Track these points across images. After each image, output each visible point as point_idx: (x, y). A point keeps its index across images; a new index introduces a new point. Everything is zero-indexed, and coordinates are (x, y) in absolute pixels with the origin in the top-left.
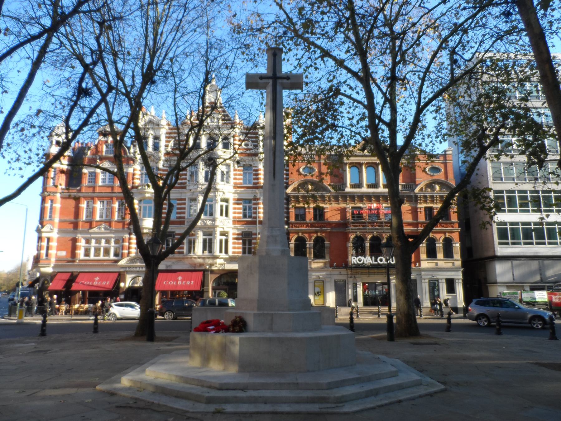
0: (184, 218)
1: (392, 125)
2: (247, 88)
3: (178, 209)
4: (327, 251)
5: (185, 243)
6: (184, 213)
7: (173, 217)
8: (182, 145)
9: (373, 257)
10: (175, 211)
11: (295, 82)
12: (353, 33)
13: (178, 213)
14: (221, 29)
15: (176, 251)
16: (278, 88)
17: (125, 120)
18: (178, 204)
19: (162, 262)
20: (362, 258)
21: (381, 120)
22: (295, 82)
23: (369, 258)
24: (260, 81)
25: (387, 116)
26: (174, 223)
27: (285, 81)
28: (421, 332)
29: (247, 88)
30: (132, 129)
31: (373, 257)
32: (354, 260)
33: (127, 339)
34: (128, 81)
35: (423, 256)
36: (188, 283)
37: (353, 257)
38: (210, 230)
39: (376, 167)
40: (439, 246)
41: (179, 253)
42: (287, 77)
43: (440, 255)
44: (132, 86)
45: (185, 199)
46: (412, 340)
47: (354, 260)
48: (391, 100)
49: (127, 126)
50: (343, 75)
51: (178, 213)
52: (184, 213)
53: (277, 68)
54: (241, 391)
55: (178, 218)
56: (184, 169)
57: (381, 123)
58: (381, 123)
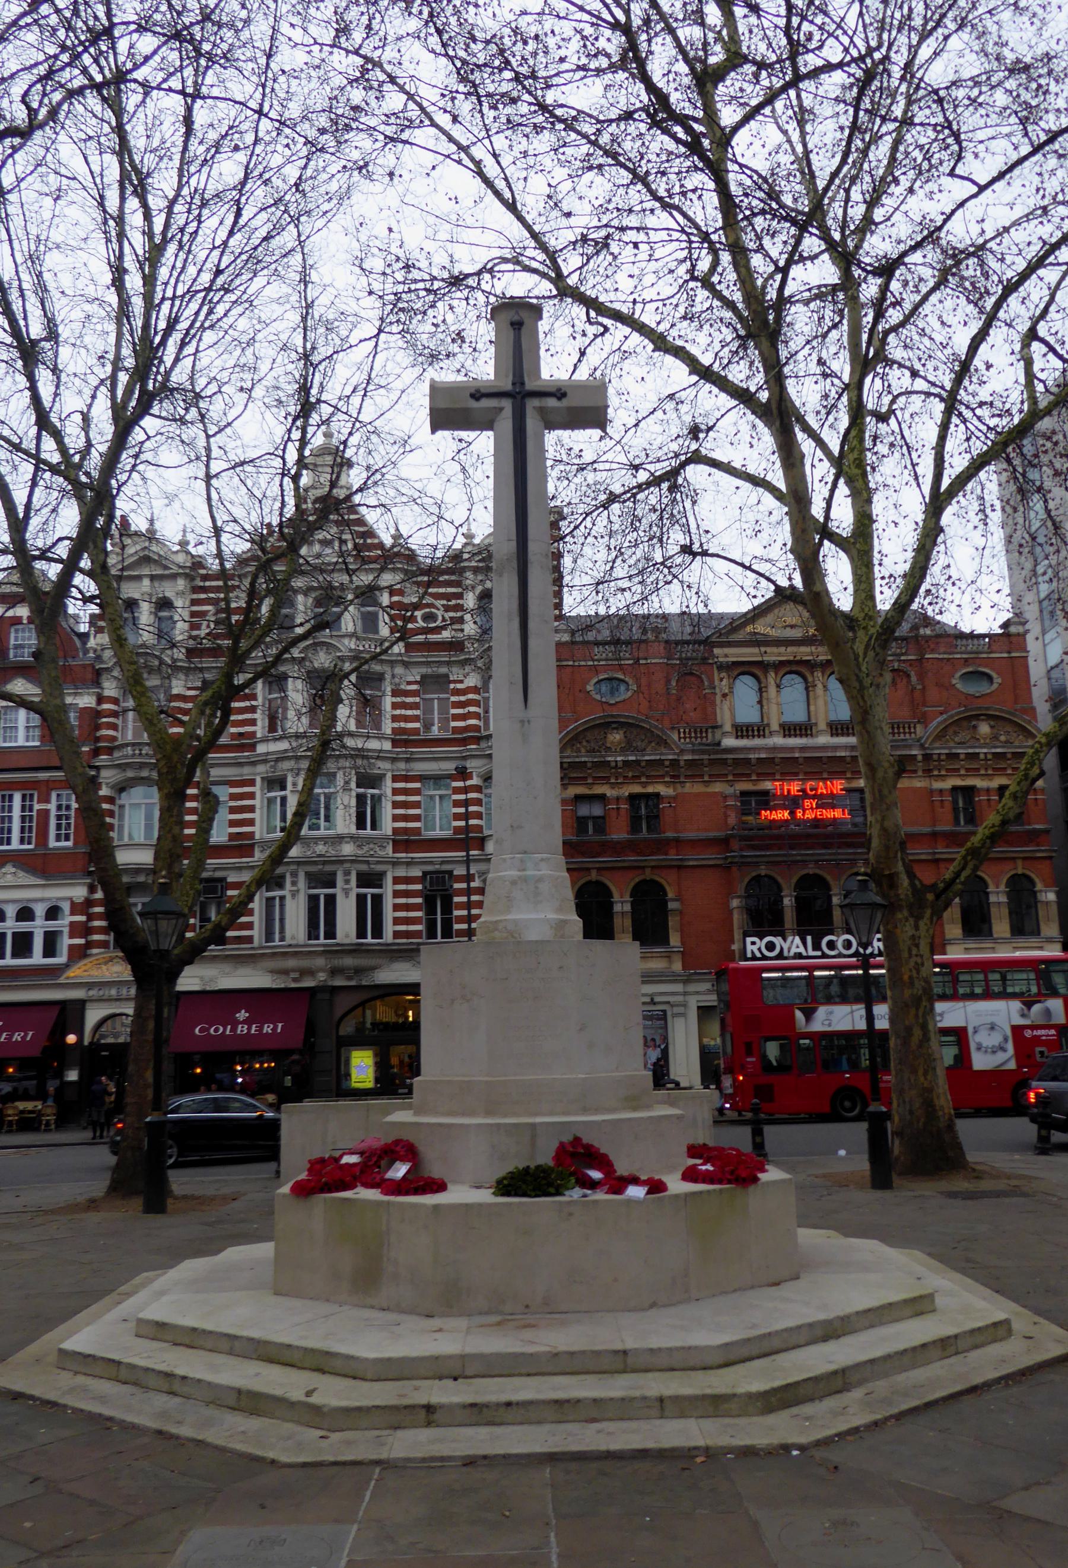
0: (252, 835)
1: (860, 545)
2: (435, 428)
3: (233, 810)
4: (673, 922)
5: (256, 912)
6: (251, 822)
7: (219, 835)
8: (237, 611)
9: (809, 938)
10: (223, 816)
11: (586, 409)
12: (193, 776)
13: (233, 823)
14: (341, 282)
15: (229, 934)
16: (532, 423)
17: (63, 550)
18: (233, 797)
19: (188, 971)
20: (777, 941)
21: (826, 532)
22: (586, 409)
23: (797, 940)
24: (474, 404)
25: (843, 517)
26: (220, 851)
27: (552, 402)
28: (971, 1157)
29: (435, 428)
30: (90, 574)
31: (809, 938)
32: (755, 948)
33: (92, 1204)
34: (74, 439)
35: (953, 930)
36: (267, 1029)
37: (749, 940)
38: (328, 868)
39: (763, 679)
40: (998, 896)
41: (239, 940)
42: (559, 392)
43: (1001, 926)
44: (86, 452)
45: (252, 783)
46: (944, 1185)
47: (755, 948)
48: (852, 467)
49: (70, 566)
50: (712, 401)
51: (233, 823)
52: (251, 822)
53: (526, 366)
54: (449, 1383)
55: (233, 837)
56: (635, 120)
57: (826, 543)
58: (826, 543)
